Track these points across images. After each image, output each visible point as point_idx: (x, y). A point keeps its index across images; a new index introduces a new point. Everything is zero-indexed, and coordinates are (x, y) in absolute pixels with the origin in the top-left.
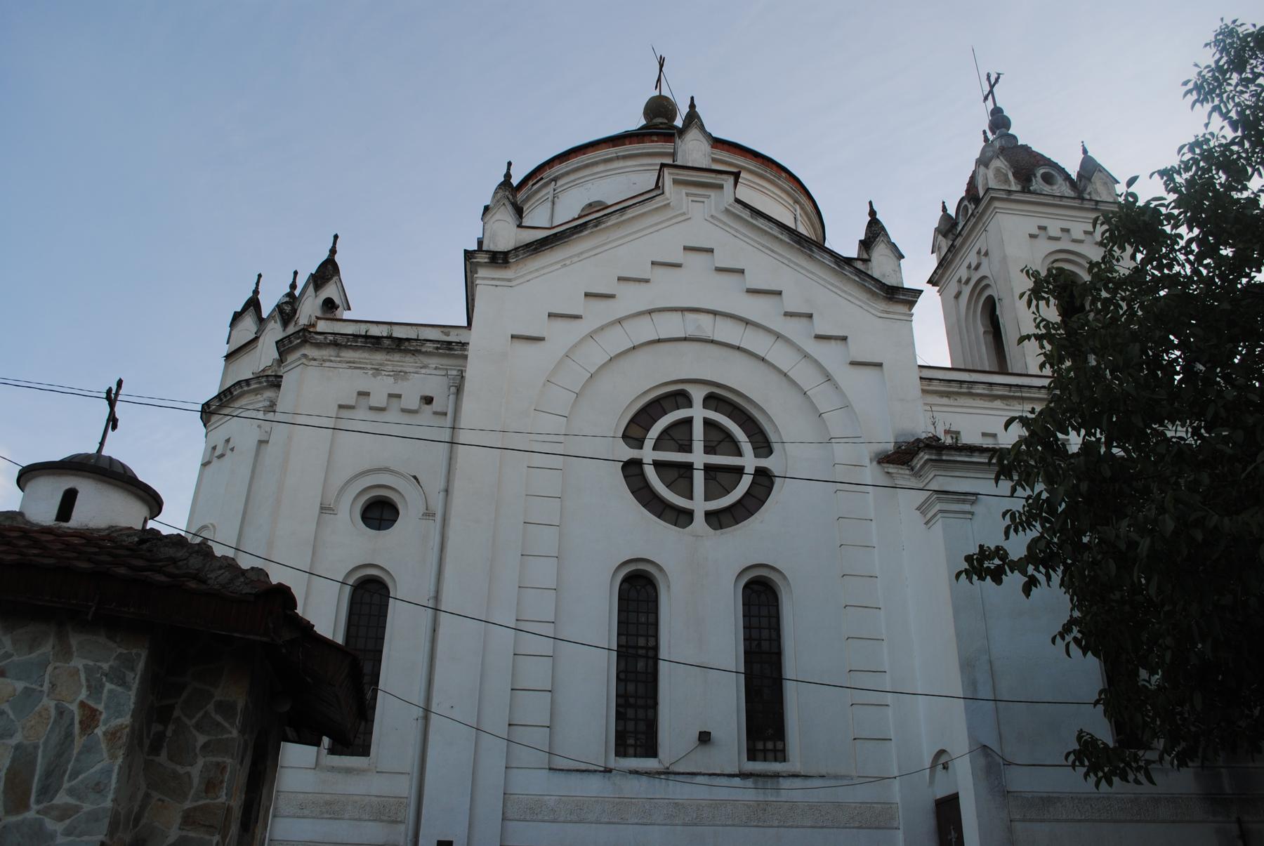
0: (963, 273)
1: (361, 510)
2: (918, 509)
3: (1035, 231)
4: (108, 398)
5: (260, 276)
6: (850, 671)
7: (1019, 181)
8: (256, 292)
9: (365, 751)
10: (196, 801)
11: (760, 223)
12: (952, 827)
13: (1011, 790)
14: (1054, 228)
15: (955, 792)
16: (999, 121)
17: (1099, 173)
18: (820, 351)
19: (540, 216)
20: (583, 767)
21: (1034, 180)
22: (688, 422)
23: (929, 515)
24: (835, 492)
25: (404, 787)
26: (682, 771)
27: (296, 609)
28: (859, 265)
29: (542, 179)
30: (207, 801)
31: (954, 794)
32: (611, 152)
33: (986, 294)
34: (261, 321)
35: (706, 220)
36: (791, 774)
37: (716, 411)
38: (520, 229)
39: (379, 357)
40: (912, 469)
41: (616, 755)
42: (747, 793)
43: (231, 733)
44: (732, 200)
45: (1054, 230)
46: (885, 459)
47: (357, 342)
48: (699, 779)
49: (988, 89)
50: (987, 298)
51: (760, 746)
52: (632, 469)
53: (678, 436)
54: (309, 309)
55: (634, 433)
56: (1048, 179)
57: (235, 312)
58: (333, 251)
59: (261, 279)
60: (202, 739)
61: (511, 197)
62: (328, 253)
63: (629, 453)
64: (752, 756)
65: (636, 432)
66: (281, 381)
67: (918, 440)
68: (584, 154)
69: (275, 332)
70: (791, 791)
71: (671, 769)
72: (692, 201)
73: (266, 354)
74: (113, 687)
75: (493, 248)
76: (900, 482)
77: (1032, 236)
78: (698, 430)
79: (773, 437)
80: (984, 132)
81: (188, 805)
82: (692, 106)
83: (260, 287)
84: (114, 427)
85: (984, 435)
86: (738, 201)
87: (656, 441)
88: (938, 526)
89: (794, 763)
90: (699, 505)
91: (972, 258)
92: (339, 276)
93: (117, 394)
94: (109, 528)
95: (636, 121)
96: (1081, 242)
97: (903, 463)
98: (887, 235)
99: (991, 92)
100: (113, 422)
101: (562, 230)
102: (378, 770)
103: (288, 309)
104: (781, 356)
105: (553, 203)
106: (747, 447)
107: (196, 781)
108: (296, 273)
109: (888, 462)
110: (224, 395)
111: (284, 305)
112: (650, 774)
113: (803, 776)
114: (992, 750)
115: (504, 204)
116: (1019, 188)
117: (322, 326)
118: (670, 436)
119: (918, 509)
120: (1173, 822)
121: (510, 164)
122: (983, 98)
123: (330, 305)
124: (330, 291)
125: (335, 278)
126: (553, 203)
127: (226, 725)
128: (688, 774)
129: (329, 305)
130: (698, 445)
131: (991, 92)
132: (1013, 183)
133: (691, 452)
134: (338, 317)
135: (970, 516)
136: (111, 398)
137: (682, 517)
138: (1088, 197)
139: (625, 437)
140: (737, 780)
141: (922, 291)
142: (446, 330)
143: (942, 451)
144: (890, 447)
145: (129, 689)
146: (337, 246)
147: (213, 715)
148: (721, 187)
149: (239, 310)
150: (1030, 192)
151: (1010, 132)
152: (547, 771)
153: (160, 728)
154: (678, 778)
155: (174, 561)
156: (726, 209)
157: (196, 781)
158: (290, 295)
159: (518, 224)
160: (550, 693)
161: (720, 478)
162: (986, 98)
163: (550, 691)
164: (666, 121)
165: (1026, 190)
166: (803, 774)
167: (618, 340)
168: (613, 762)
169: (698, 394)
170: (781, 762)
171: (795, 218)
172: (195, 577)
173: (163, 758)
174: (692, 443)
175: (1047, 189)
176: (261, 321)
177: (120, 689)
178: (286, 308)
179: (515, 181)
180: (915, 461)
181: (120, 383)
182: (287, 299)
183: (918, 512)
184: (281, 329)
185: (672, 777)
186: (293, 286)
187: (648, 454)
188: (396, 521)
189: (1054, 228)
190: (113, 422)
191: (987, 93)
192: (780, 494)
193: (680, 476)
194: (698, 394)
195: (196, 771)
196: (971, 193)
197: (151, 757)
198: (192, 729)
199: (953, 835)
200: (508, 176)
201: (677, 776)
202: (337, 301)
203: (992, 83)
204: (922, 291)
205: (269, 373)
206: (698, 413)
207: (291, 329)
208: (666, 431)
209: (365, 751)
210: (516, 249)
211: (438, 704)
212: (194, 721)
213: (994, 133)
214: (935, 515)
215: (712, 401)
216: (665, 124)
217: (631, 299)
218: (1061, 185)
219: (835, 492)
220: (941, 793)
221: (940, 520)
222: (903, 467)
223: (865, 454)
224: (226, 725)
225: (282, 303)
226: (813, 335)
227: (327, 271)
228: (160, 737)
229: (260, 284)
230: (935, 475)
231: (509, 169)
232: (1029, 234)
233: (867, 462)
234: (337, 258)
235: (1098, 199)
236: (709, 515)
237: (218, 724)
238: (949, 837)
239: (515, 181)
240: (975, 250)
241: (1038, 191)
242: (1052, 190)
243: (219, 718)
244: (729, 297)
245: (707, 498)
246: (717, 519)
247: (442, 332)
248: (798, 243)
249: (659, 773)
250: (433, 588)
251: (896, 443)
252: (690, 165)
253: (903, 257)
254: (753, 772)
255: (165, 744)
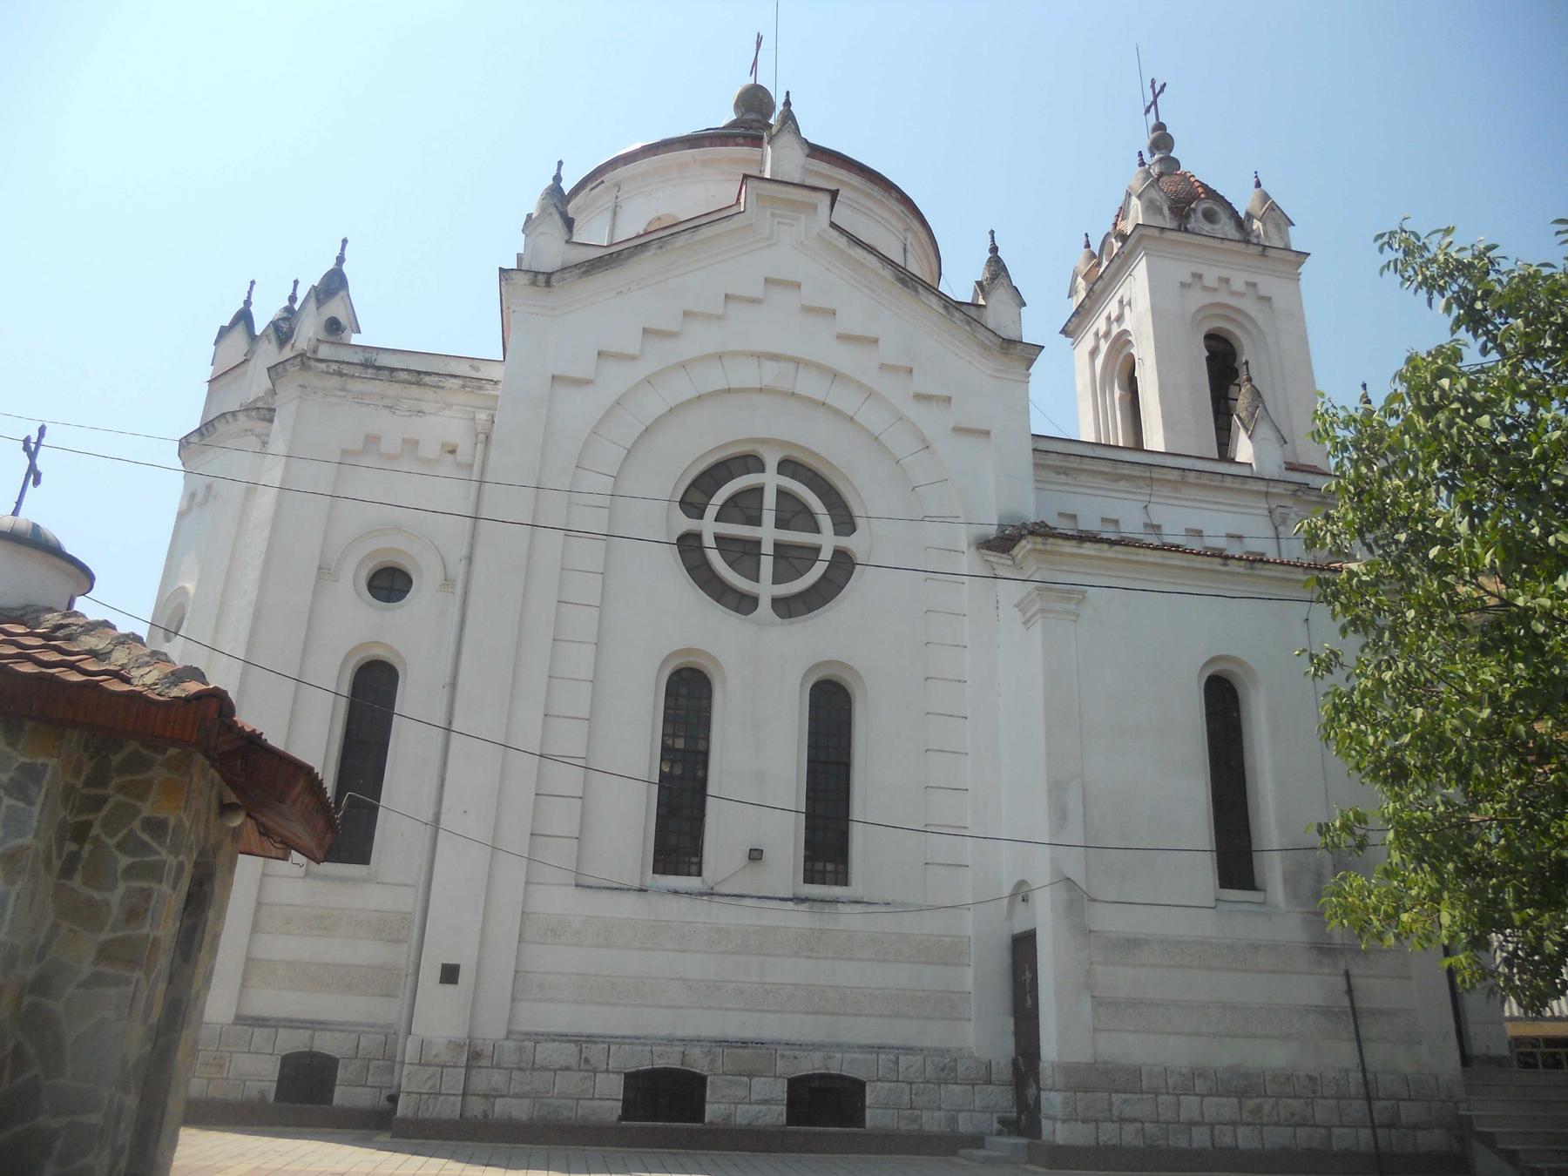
0: (1100, 324)
1: (370, 571)
2: (1017, 606)
3: (1188, 279)
4: (26, 448)
5: (253, 283)
6: (926, 787)
7: (1176, 216)
8: (248, 303)
9: (364, 859)
10: (115, 931)
11: (859, 253)
12: (1027, 966)
13: (1094, 929)
14: (1211, 275)
15: (1033, 927)
16: (1162, 141)
17: (1272, 211)
18: (914, 412)
19: (595, 232)
20: (615, 885)
21: (1193, 215)
22: (758, 491)
23: (1028, 615)
24: (925, 581)
25: (407, 901)
26: (728, 892)
27: (234, 716)
28: (973, 312)
29: (603, 182)
30: (129, 932)
31: (1029, 931)
32: (689, 154)
33: (1125, 352)
34: (253, 338)
35: (794, 247)
36: (852, 900)
37: (792, 478)
38: (567, 245)
39: (394, 389)
40: (1013, 559)
41: (653, 873)
42: (799, 919)
43: (159, 854)
44: (826, 224)
45: (1210, 278)
46: (986, 544)
47: (367, 373)
48: (747, 902)
49: (1151, 98)
50: (1125, 356)
51: (819, 866)
52: (689, 545)
53: (745, 507)
54: (308, 331)
55: (693, 499)
56: (1210, 216)
57: (222, 327)
58: (341, 259)
59: (255, 287)
60: (124, 861)
61: (559, 205)
62: (335, 261)
63: (686, 524)
64: (810, 878)
65: (697, 497)
66: (274, 416)
67: (1024, 525)
68: (655, 155)
69: (269, 354)
70: (850, 920)
71: (718, 889)
72: (779, 223)
73: (256, 383)
74: (13, 802)
75: (535, 268)
76: (1000, 573)
77: (1183, 285)
78: (770, 500)
79: (856, 510)
80: (1140, 154)
81: (105, 935)
82: (787, 103)
83: (252, 297)
84: (37, 482)
85: (1104, 520)
86: (833, 225)
87: (720, 510)
88: (1037, 630)
89: (856, 888)
90: (766, 589)
91: (1112, 308)
92: (347, 290)
93: (38, 444)
94: (23, 608)
95: (724, 115)
96: (1242, 295)
97: (1003, 552)
98: (1008, 276)
99: (1155, 103)
100: (34, 475)
101: (618, 250)
102: (379, 881)
103: (285, 326)
104: (872, 418)
105: (615, 214)
106: (825, 521)
107: (115, 909)
108: (296, 282)
109: (989, 548)
110: (207, 429)
111: (280, 321)
112: (691, 894)
113: (866, 903)
114: (1076, 884)
115: (551, 214)
116: (1174, 225)
117: (324, 351)
118: (735, 503)
119: (1017, 606)
120: (1273, 972)
121: (560, 163)
122: (1144, 112)
123: (334, 327)
124: (334, 308)
125: (342, 293)
126: (615, 214)
127: (154, 844)
128: (735, 896)
129: (334, 326)
130: (769, 517)
131: (1155, 103)
132: (1168, 217)
133: (760, 526)
134: (345, 342)
135: (1074, 618)
136: (31, 449)
137: (744, 603)
138: (1255, 241)
139: (684, 503)
140: (790, 905)
141: (1043, 347)
142: (476, 363)
143: (1047, 539)
144: (992, 531)
145: (31, 803)
146: (346, 253)
147: (139, 833)
148: (815, 207)
149: (227, 324)
150: (1187, 230)
151: (1171, 155)
152: (572, 889)
153: (73, 847)
154: (723, 900)
155: (94, 654)
156: (819, 235)
157: (115, 909)
158: (289, 310)
159: (567, 238)
160: (580, 801)
161: (791, 559)
162: (1148, 111)
163: (581, 798)
164: (760, 117)
165: (1182, 228)
166: (865, 900)
167: (680, 389)
168: (652, 880)
169: (771, 461)
170: (841, 885)
171: (905, 249)
172: (116, 675)
173: (76, 882)
174: (761, 514)
175: (1207, 227)
176: (253, 338)
177: (21, 804)
178: (283, 325)
179: (567, 186)
180: (1017, 549)
181: (42, 431)
182: (285, 315)
183: (1017, 609)
184: (277, 351)
185: (716, 899)
186: (293, 298)
187: (709, 527)
188: (408, 591)
189: (1211, 275)
190: (34, 475)
191: (1149, 104)
192: (861, 580)
193: (745, 553)
194: (771, 461)
195: (116, 897)
196: (1118, 228)
197: (62, 881)
198: (113, 849)
199: (1028, 975)
200: (557, 178)
201: (722, 898)
202: (343, 320)
203: (1157, 92)
204: (1043, 347)
205: (259, 404)
206: (771, 481)
207: (288, 353)
208: (732, 500)
209: (364, 859)
210: (563, 269)
211: (449, 809)
212: (115, 840)
213: (1153, 155)
214: (1035, 615)
215: (789, 466)
216: (759, 121)
217: (701, 340)
218: (1225, 224)
219: (925, 581)
220: (1020, 927)
221: (1040, 621)
222: (1003, 555)
223: (963, 537)
224: (154, 844)
225: (279, 319)
226: (911, 393)
227: (334, 283)
228: (73, 859)
229: (253, 293)
230: (1039, 568)
231: (559, 169)
232: (1181, 283)
233: (964, 545)
234: (346, 268)
235: (1267, 244)
236: (776, 602)
237: (145, 845)
238: (1023, 978)
239: (567, 186)
240: (1117, 297)
241: (1197, 231)
242: (1214, 230)
243: (146, 837)
244: (818, 344)
245: (776, 580)
246: (787, 608)
247: (471, 366)
248: (902, 281)
249: (701, 894)
250: (449, 672)
251: (1000, 525)
252: (780, 179)
253: (1025, 305)
254: (809, 896)
255: (80, 867)
